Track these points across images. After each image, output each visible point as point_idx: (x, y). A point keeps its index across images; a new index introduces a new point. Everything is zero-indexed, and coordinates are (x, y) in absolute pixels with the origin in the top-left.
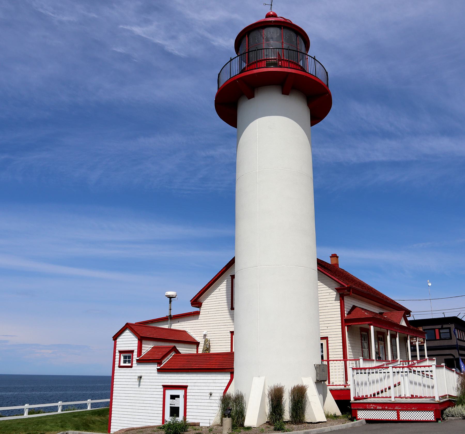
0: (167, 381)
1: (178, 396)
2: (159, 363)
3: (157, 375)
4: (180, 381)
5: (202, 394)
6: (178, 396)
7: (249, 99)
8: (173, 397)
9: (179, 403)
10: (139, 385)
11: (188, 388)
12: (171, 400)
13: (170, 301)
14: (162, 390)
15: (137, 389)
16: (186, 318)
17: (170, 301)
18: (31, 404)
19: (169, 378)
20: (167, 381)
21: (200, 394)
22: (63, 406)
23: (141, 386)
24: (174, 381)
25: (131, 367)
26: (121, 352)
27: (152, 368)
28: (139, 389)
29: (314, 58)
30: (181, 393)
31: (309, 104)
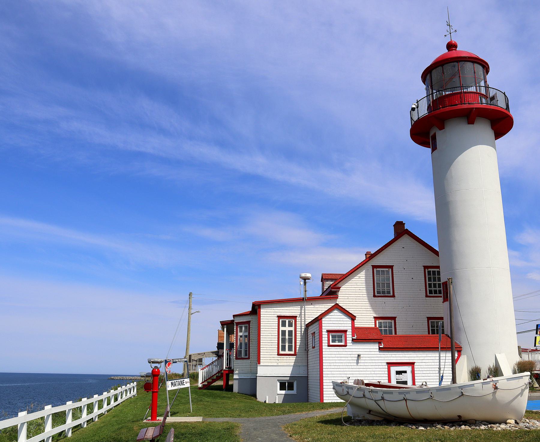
0: (392, 358)
1: (405, 372)
2: (380, 343)
3: (378, 353)
4: (403, 358)
5: (430, 369)
6: (405, 372)
7: (468, 124)
8: (398, 373)
9: (408, 377)
10: (358, 363)
11: (415, 364)
12: (397, 375)
13: (305, 283)
14: (386, 367)
15: (355, 367)
16: (278, 305)
17: (305, 283)
18: (32, 412)
19: (394, 356)
20: (392, 358)
21: (428, 369)
22: (30, 424)
23: (359, 364)
24: (400, 358)
25: (345, 346)
26: (329, 332)
27: (375, 347)
28: (358, 367)
29: (504, 94)
30: (408, 369)
31: (493, 127)
